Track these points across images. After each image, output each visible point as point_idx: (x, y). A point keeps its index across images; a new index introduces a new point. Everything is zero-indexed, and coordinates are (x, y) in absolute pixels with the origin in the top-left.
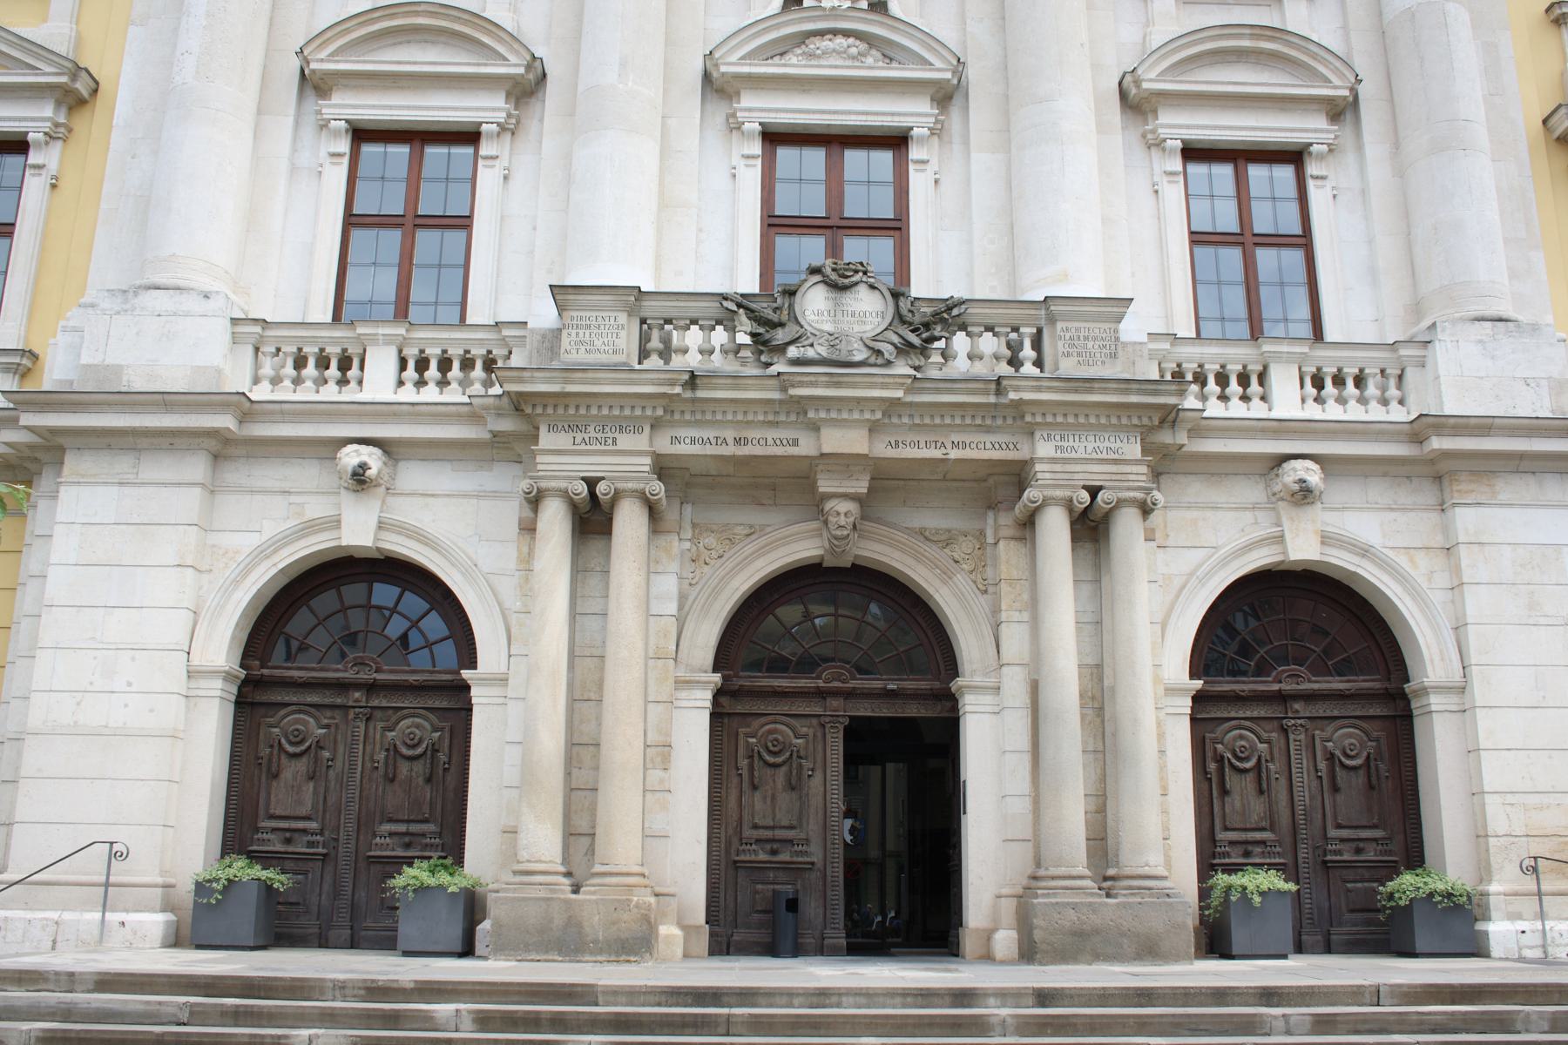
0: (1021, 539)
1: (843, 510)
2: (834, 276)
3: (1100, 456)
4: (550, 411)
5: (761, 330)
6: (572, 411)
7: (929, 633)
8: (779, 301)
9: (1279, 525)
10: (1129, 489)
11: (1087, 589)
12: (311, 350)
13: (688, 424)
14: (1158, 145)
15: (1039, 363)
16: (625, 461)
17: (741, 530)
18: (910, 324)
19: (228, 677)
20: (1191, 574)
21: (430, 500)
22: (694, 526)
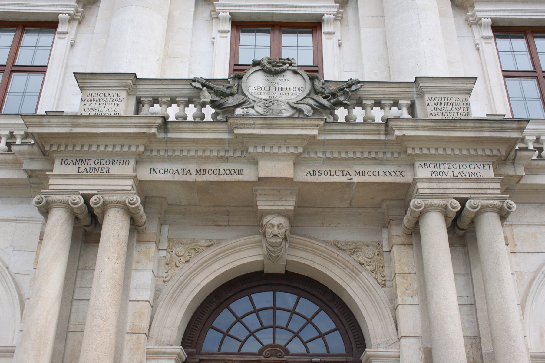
0: (410, 245)
1: (276, 224)
2: (268, 66)
4: (62, 148)
5: (218, 99)
6: (78, 148)
7: (344, 321)
8: (231, 83)
10: (489, 199)
11: (461, 279)
13: (163, 160)
14: (476, 24)
16: (115, 183)
18: (322, 93)
22: (169, 240)
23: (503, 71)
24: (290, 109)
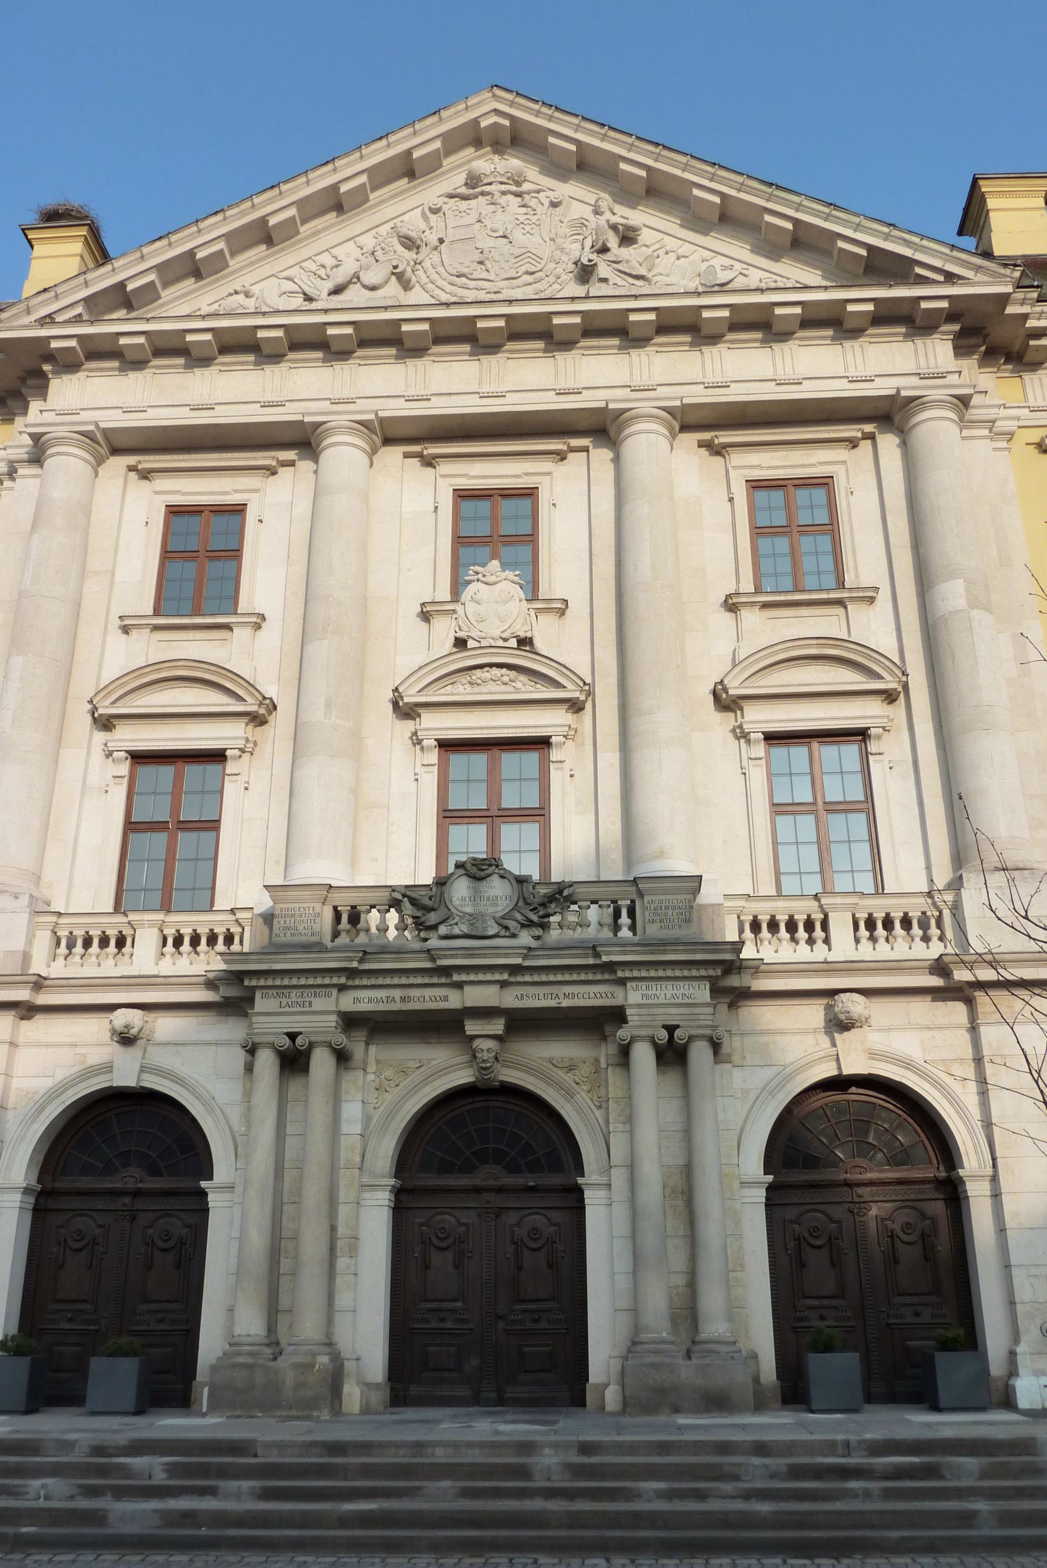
3: (677, 1001)
9: (834, 1045)
12: (95, 933)
15: (633, 928)
16: (317, 1016)
17: (413, 1064)
18: (530, 904)
19: (27, 1191)
20: (763, 1089)
21: (181, 1048)
22: (378, 1062)
23: (774, 805)
24: (496, 926)
